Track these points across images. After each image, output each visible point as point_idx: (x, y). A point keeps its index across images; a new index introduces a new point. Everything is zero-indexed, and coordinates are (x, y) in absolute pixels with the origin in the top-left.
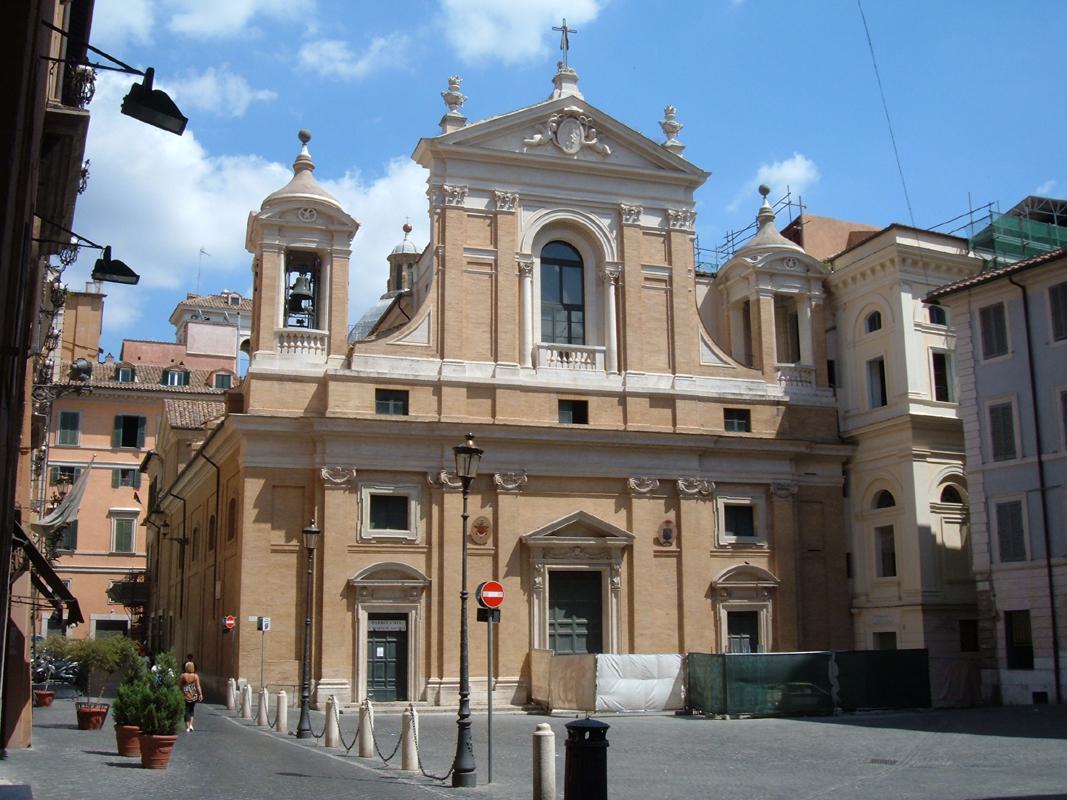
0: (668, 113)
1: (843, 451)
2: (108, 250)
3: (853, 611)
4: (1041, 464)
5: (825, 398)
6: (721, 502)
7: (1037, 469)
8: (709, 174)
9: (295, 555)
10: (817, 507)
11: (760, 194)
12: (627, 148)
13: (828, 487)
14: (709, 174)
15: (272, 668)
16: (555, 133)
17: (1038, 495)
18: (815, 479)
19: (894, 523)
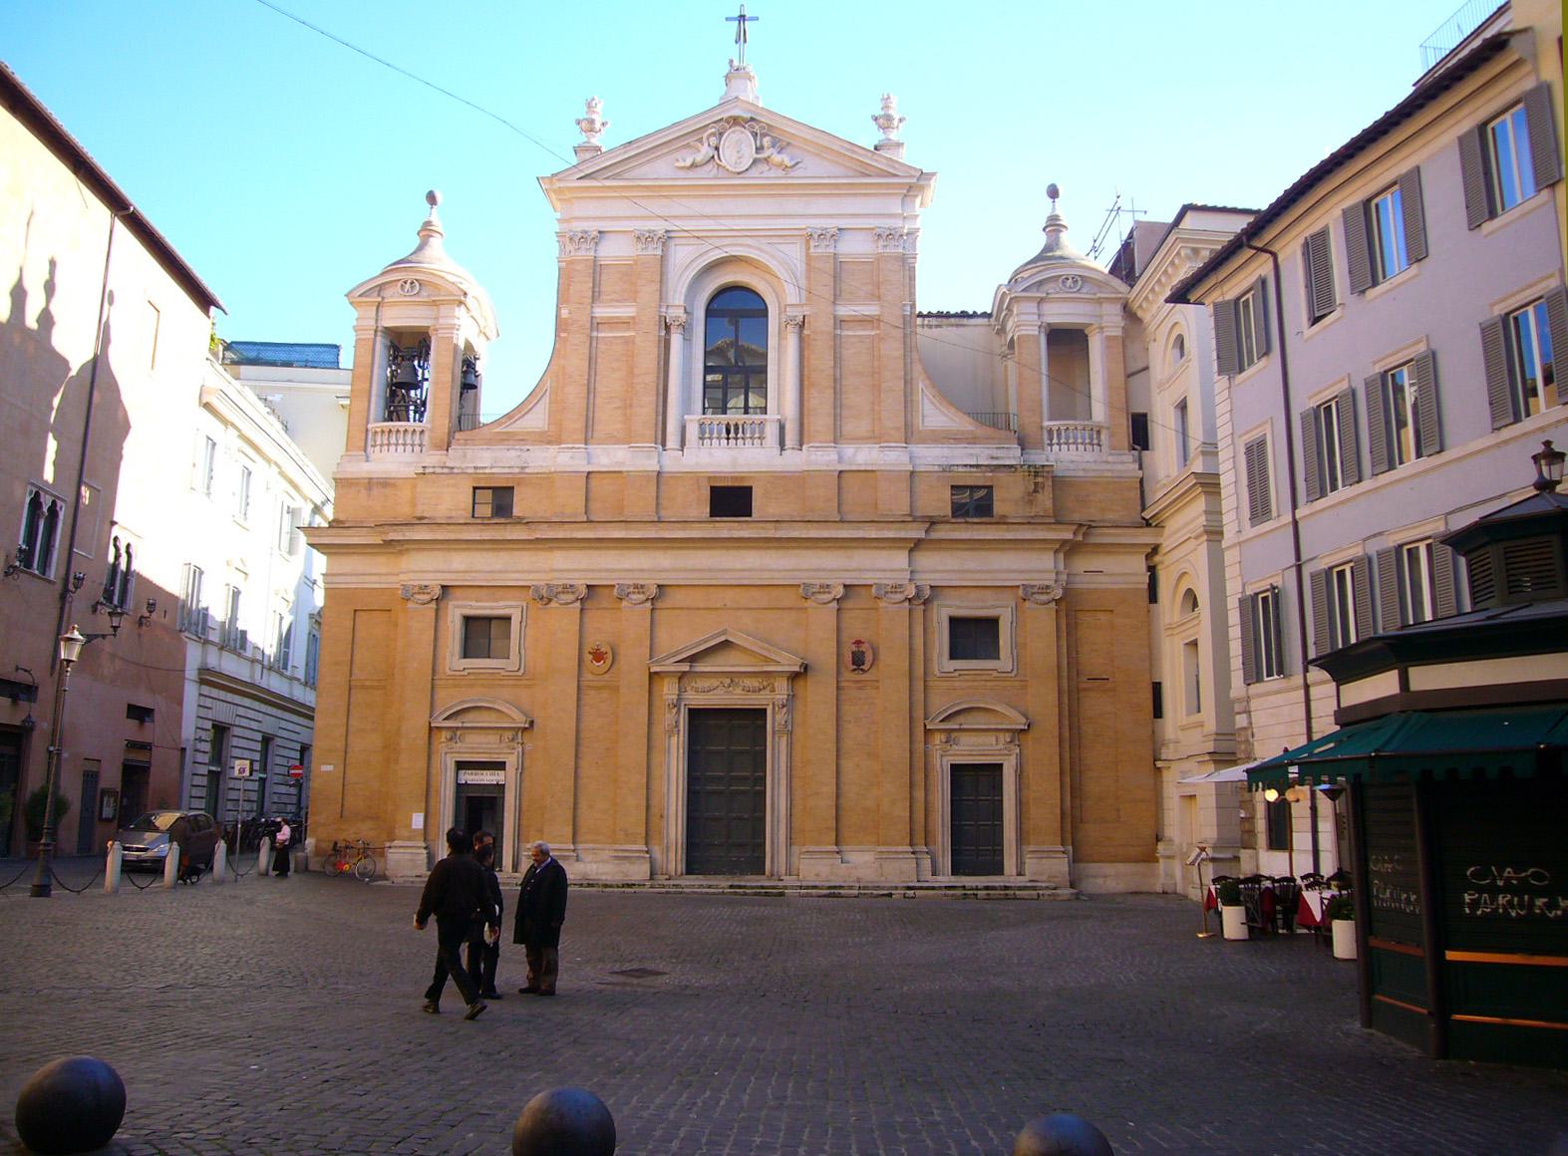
0: (886, 101)
1: (1146, 537)
2: (1536, 458)
3: (1159, 764)
4: (1295, 523)
5: (1125, 464)
6: (511, 664)
7: (1290, 529)
8: (934, 174)
9: (206, 778)
10: (1104, 617)
11: (1048, 198)
12: (818, 155)
13: (1121, 590)
14: (934, 174)
15: (510, 876)
16: (717, 149)
17: (1293, 572)
18: (1100, 578)
19: (125, 719)
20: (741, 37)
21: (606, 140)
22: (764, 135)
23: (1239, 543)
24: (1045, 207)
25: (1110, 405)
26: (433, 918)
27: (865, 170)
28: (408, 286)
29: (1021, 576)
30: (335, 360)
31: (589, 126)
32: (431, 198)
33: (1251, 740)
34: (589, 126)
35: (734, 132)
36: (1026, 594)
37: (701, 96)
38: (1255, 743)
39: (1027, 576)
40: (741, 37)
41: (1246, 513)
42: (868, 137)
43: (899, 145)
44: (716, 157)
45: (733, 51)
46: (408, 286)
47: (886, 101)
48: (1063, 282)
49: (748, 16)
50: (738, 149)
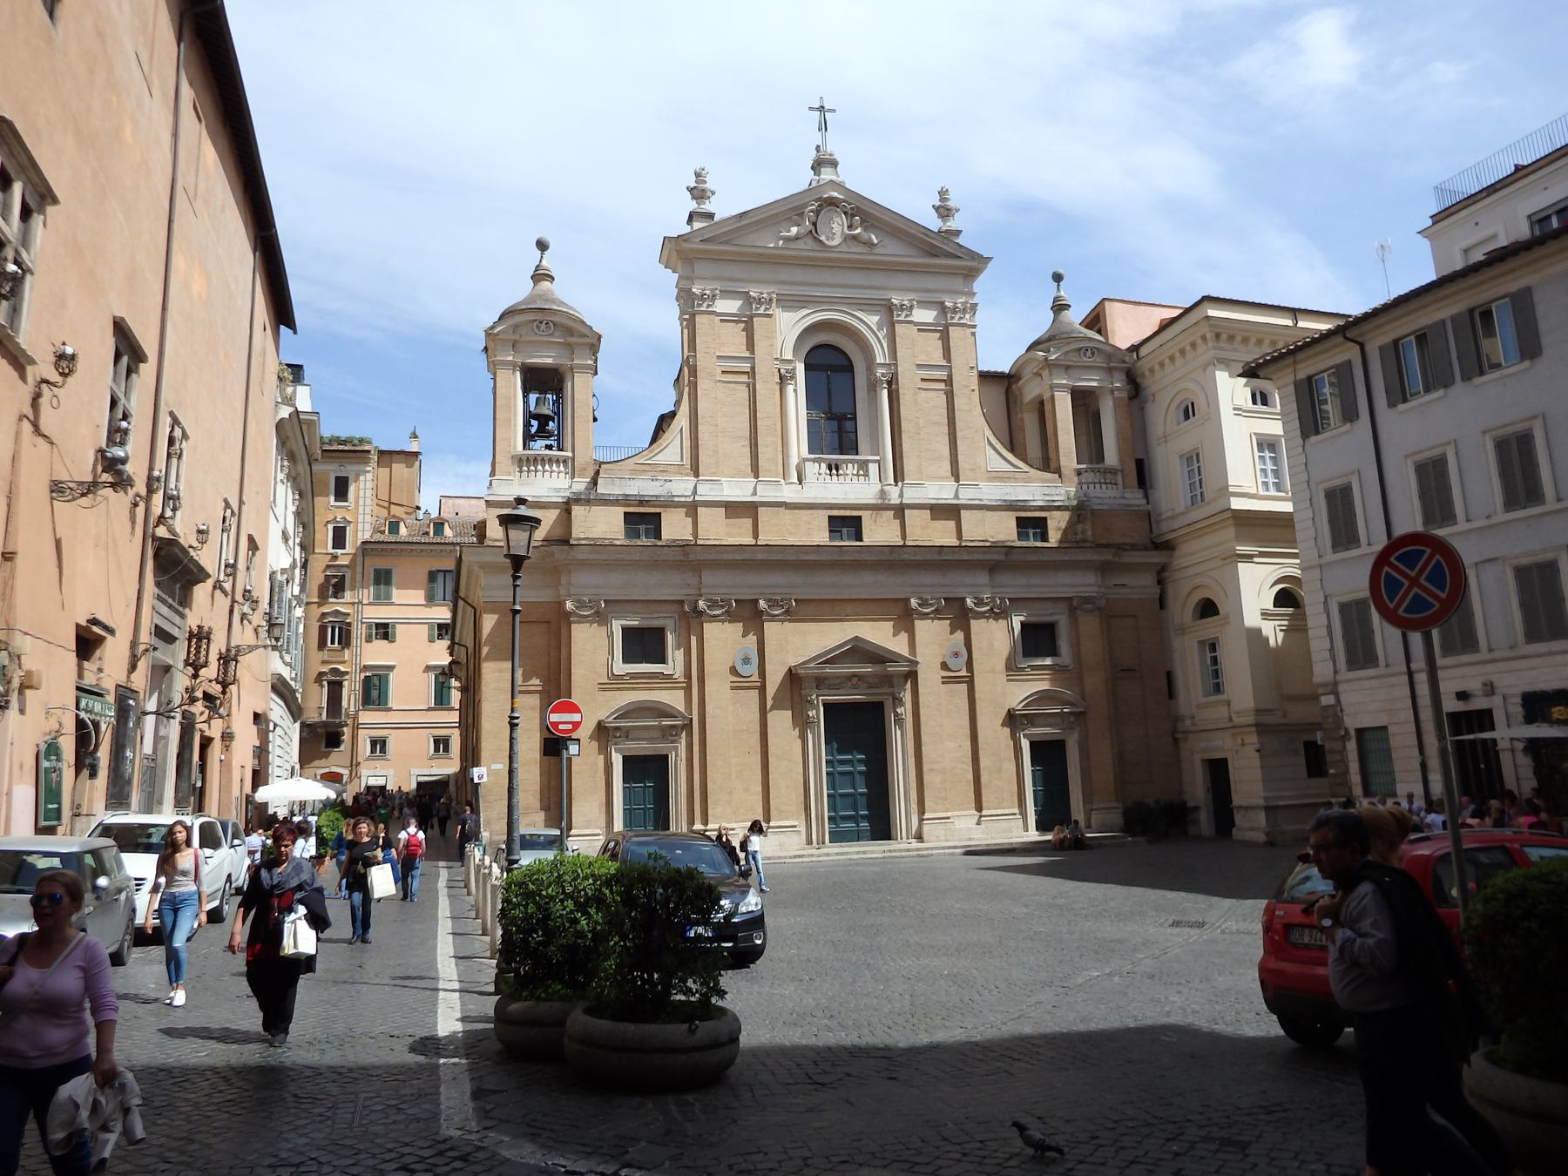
0: (943, 194)
1: (1156, 558)
3: (1176, 736)
5: (1135, 498)
20: (824, 126)
21: (723, 206)
22: (853, 216)
23: (1321, 566)
24: (1051, 290)
25: (1120, 451)
26: (271, 927)
27: (933, 252)
28: (543, 326)
29: (1072, 589)
30: (852, 411)
31: (699, 193)
32: (542, 246)
33: (1340, 714)
34: (699, 193)
35: (829, 211)
36: (1073, 606)
37: (796, 179)
38: (1345, 718)
39: (1077, 589)
40: (824, 126)
41: (1328, 542)
42: (933, 223)
43: (958, 233)
44: (814, 232)
45: (817, 138)
46: (543, 326)
47: (943, 194)
48: (537, 326)
49: (826, 108)
50: (836, 229)
